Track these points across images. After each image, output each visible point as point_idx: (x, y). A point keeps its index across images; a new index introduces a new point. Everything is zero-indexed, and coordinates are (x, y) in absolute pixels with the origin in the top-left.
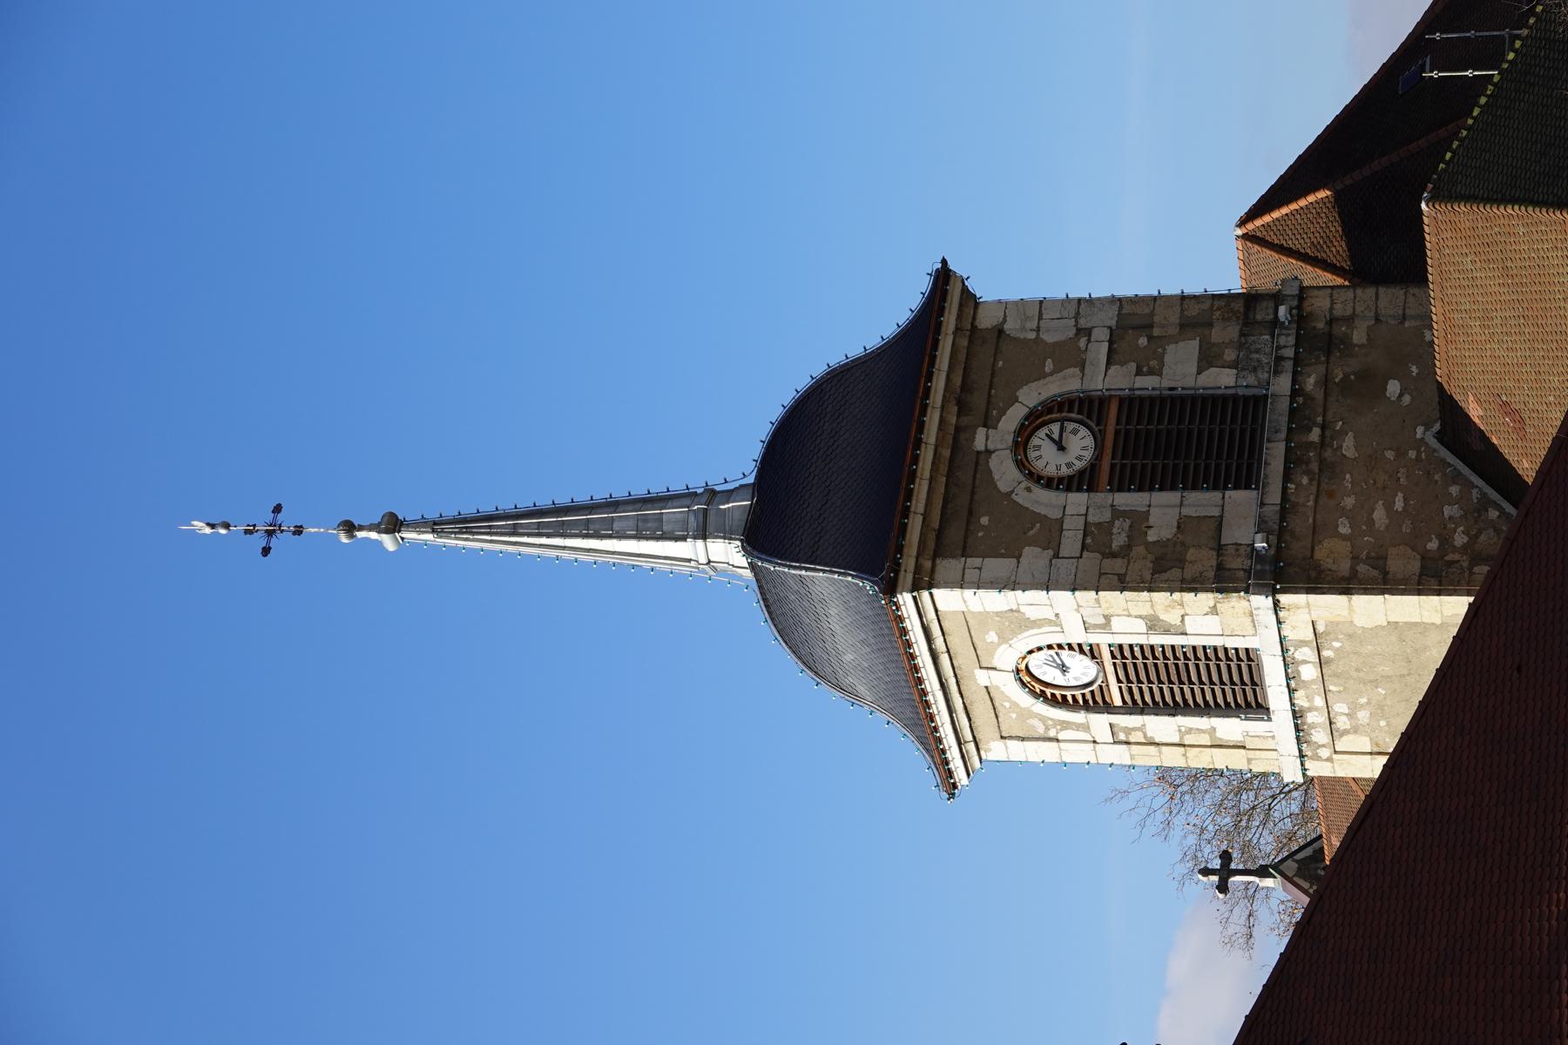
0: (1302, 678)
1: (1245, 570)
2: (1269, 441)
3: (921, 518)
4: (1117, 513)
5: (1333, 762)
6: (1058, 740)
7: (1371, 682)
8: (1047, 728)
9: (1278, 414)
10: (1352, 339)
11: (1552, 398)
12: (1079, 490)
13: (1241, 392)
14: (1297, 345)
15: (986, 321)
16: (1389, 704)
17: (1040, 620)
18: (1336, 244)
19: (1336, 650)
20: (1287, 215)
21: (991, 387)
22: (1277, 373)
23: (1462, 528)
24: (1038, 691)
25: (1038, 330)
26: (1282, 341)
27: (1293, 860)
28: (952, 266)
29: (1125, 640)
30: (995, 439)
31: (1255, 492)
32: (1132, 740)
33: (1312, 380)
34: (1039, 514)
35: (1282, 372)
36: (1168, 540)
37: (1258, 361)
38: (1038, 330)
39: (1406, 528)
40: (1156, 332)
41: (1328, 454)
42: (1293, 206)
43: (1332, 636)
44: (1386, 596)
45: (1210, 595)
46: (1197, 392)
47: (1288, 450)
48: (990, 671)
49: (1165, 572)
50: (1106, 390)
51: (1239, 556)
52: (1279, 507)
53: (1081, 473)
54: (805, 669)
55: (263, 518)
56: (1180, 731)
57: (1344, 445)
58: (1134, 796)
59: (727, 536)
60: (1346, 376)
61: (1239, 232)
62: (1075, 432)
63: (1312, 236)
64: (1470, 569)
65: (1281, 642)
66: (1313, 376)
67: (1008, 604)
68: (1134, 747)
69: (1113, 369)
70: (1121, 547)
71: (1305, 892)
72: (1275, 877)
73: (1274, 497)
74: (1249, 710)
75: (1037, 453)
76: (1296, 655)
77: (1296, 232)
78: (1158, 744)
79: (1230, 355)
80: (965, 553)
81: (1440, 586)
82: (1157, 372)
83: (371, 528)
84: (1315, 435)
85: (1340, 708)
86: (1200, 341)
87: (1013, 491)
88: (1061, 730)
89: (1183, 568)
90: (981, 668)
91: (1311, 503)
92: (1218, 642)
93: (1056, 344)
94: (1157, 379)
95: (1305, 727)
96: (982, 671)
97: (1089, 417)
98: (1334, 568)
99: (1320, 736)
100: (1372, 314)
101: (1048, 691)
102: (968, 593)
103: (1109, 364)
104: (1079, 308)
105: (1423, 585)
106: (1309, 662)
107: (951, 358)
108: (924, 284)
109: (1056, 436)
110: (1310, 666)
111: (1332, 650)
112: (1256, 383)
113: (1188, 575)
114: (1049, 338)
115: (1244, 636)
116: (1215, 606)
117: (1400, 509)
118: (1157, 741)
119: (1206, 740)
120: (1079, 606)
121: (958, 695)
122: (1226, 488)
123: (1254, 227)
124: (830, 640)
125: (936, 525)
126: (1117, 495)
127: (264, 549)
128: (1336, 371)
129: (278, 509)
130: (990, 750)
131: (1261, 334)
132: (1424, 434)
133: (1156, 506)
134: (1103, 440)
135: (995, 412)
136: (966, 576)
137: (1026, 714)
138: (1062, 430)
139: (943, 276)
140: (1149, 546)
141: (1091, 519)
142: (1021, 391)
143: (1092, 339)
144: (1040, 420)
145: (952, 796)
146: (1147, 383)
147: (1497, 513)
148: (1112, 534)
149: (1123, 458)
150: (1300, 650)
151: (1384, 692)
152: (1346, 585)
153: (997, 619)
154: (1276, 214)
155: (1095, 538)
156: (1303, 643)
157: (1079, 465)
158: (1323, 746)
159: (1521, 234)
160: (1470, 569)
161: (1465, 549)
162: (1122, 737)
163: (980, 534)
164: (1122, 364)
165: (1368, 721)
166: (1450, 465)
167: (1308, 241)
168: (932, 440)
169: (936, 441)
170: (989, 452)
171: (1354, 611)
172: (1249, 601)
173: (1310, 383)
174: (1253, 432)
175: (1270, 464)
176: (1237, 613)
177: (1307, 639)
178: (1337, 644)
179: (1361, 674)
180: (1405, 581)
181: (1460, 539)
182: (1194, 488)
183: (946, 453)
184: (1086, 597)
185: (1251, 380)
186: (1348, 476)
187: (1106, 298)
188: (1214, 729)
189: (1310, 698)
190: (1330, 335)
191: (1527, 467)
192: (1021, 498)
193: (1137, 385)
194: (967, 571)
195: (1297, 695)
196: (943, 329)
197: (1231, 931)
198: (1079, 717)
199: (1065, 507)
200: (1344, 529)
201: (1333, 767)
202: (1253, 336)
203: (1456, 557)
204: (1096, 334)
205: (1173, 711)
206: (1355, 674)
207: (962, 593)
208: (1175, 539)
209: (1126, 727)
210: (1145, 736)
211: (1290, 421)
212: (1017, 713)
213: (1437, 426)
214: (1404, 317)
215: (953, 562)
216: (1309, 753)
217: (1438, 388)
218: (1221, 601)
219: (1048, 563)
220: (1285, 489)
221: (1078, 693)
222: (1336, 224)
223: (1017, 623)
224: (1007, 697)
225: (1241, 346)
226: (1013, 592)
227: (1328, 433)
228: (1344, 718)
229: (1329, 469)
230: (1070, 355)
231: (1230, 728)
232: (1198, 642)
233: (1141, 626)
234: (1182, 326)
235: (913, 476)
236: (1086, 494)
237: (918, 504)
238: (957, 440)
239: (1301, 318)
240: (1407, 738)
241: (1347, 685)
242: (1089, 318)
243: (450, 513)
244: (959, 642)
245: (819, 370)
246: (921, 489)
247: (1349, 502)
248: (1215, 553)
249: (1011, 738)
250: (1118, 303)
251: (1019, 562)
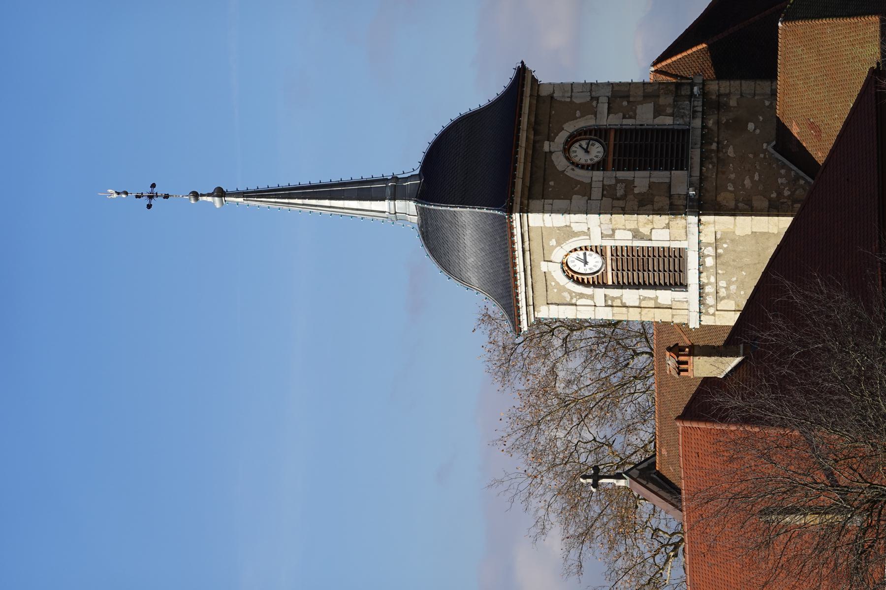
0: (706, 265)
1: (684, 206)
2: (692, 148)
3: (521, 180)
4: (618, 181)
5: (715, 316)
6: (576, 305)
7: (739, 268)
8: (572, 298)
10: (729, 103)
11: (836, 116)
12: (598, 170)
13: (676, 127)
14: (703, 106)
16: (747, 281)
17: (580, 232)
18: (708, 72)
19: (725, 249)
20: (680, 58)
21: (549, 123)
22: (694, 118)
23: (787, 188)
24: (570, 276)
25: (571, 97)
26: (696, 103)
27: (636, 469)
31: (686, 172)
32: (614, 305)
33: (711, 122)
34: (579, 181)
35: (696, 118)
36: (644, 192)
37: (684, 113)
38: (571, 97)
39: (761, 188)
40: (631, 99)
41: (721, 155)
42: (684, 54)
43: (723, 241)
44: (753, 217)
45: (667, 217)
46: (654, 127)
47: (702, 152)
48: (549, 263)
49: (645, 206)
50: (609, 125)
51: (680, 199)
52: (698, 178)
53: (599, 163)
54: (443, 271)
55: (147, 190)
56: (640, 298)
57: (729, 151)
58: (507, 484)
61: (653, 69)
62: (593, 145)
63: (694, 69)
64: (792, 205)
65: (699, 243)
66: (712, 120)
67: (565, 222)
68: (615, 308)
69: (611, 116)
72: (625, 479)
73: (696, 173)
74: (676, 287)
75: (575, 154)
76: (705, 252)
77: (685, 67)
78: (627, 307)
79: (669, 110)
80: (543, 197)
81: (778, 212)
83: (209, 195)
84: (714, 146)
85: (722, 284)
86: (654, 104)
87: (565, 170)
88: (579, 299)
89: (653, 205)
90: (544, 261)
91: (714, 176)
93: (581, 104)
94: (634, 120)
95: (704, 295)
96: (545, 262)
97: (600, 137)
98: (727, 204)
99: (710, 300)
100: (739, 93)
101: (575, 276)
102: (547, 216)
103: (609, 113)
104: (591, 87)
105: (770, 212)
106: (711, 256)
107: (529, 108)
108: (512, 74)
110: (711, 258)
111: (722, 249)
112: (683, 123)
114: (577, 101)
115: (680, 241)
116: (669, 223)
117: (757, 180)
118: (627, 305)
120: (601, 223)
121: (530, 276)
122: (671, 170)
123: (661, 66)
124: (462, 250)
126: (617, 172)
127: (148, 205)
128: (723, 118)
130: (540, 311)
131: (684, 101)
132: (767, 146)
133: (637, 178)
134: (608, 148)
135: (552, 134)
136: (545, 208)
137: (563, 289)
138: (588, 144)
139: (522, 71)
141: (605, 183)
142: (565, 125)
143: (599, 102)
144: (575, 139)
147: (804, 182)
148: (616, 190)
149: (619, 157)
150: (707, 248)
151: (745, 274)
152: (734, 212)
153: (558, 231)
154: (674, 59)
155: (608, 192)
156: (709, 244)
157: (596, 160)
158: (711, 306)
159: (829, 32)
160: (792, 205)
161: (789, 197)
162: (610, 303)
163: (550, 189)
164: (615, 113)
165: (735, 291)
166: (780, 161)
167: (692, 71)
169: (526, 145)
170: (551, 153)
171: (736, 225)
172: (686, 220)
173: (710, 123)
174: (683, 146)
175: (693, 159)
176: (679, 227)
177: (712, 242)
178: (725, 246)
179: (735, 263)
180: (761, 210)
182: (655, 169)
183: (530, 152)
184: (605, 218)
185: (681, 121)
186: (731, 165)
187: (605, 83)
188: (657, 297)
189: (708, 278)
191: (820, 156)
192: (569, 173)
193: (624, 123)
194: (545, 205)
195: (702, 275)
196: (524, 94)
197: (569, 562)
198: (588, 291)
199: (592, 178)
200: (731, 188)
201: (715, 319)
202: (681, 101)
203: (785, 200)
204: (601, 100)
205: (638, 287)
206: (732, 263)
207: (543, 216)
208: (648, 192)
209: (613, 297)
210: (622, 302)
211: (702, 140)
212: (557, 289)
213: (774, 143)
214: (755, 95)
215: (538, 201)
216: (704, 311)
217: (777, 121)
218: (672, 220)
219: (586, 202)
220: (701, 170)
221: (590, 277)
222: (708, 62)
223: (567, 233)
224: (554, 278)
226: (569, 215)
227: (720, 146)
228: (723, 290)
230: (589, 109)
231: (665, 296)
233: (629, 235)
234: (644, 97)
235: (516, 161)
236: (602, 172)
238: (535, 148)
240: (750, 302)
241: (727, 270)
242: (597, 92)
244: (536, 246)
245: (455, 116)
246: (520, 167)
248: (668, 199)
249: (552, 304)
250: (611, 85)
251: (571, 202)
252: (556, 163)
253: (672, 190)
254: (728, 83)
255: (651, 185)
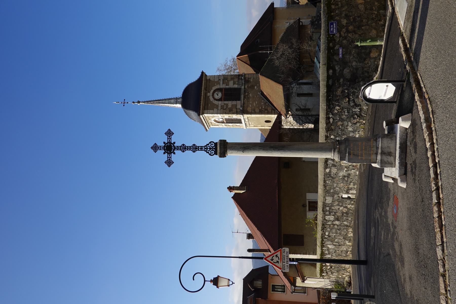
4: (225, 104)
9: (242, 91)
12: (220, 101)
15: (208, 78)
22: (242, 86)
28: (203, 71)
29: (226, 118)
30: (210, 94)
40: (228, 80)
41: (248, 96)
59: (179, 104)
60: (250, 86)
62: (219, 93)
69: (223, 85)
70: (225, 108)
71: (261, 281)
73: (242, 102)
82: (228, 85)
83: (136, 102)
92: (237, 118)
93: (216, 81)
108: (200, 73)
109: (217, 94)
113: (233, 112)
119: (235, 125)
125: (204, 106)
129: (125, 100)
138: (218, 93)
139: (203, 73)
140: (228, 108)
145: (207, 131)
146: (227, 87)
157: (220, 97)
164: (224, 84)
168: (203, 95)
170: (209, 96)
173: (246, 87)
180: (257, 113)
181: (263, 107)
183: (204, 96)
184: (222, 115)
190: (248, 80)
192: (213, 102)
200: (250, 106)
203: (263, 109)
213: (261, 93)
220: (244, 101)
225: (238, 82)
227: (248, 93)
229: (248, 98)
232: (235, 118)
237: (202, 104)
238: (206, 94)
239: (245, 78)
243: (146, 101)
245: (188, 84)
246: (202, 102)
247: (251, 102)
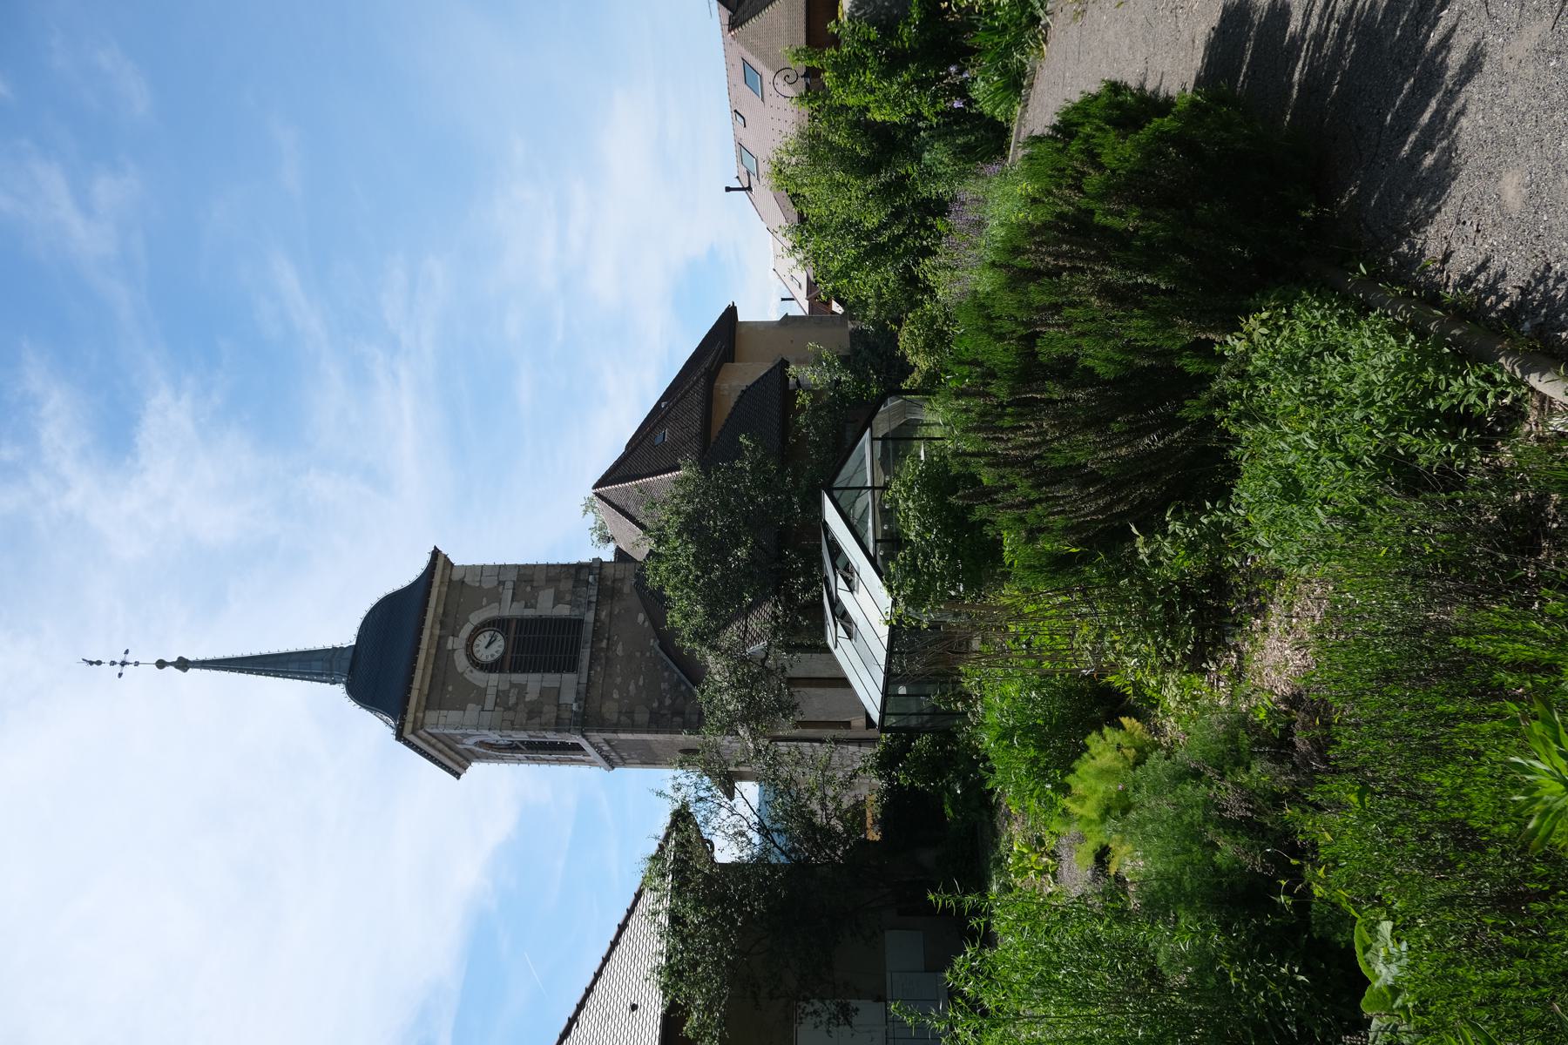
4: (512, 685)
22: (588, 610)
33: (604, 613)
40: (535, 584)
47: (592, 652)
69: (515, 603)
79: (568, 597)
84: (604, 644)
103: (512, 601)
108: (428, 557)
114: (485, 586)
139: (436, 553)
170: (454, 650)
183: (433, 651)
192: (468, 676)
200: (616, 696)
252: (457, 663)
253: (561, 698)
254: (623, 566)
255: (543, 691)
